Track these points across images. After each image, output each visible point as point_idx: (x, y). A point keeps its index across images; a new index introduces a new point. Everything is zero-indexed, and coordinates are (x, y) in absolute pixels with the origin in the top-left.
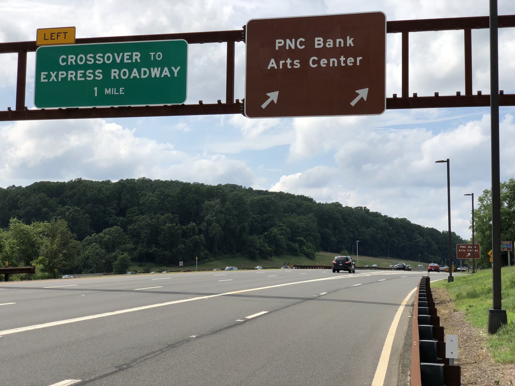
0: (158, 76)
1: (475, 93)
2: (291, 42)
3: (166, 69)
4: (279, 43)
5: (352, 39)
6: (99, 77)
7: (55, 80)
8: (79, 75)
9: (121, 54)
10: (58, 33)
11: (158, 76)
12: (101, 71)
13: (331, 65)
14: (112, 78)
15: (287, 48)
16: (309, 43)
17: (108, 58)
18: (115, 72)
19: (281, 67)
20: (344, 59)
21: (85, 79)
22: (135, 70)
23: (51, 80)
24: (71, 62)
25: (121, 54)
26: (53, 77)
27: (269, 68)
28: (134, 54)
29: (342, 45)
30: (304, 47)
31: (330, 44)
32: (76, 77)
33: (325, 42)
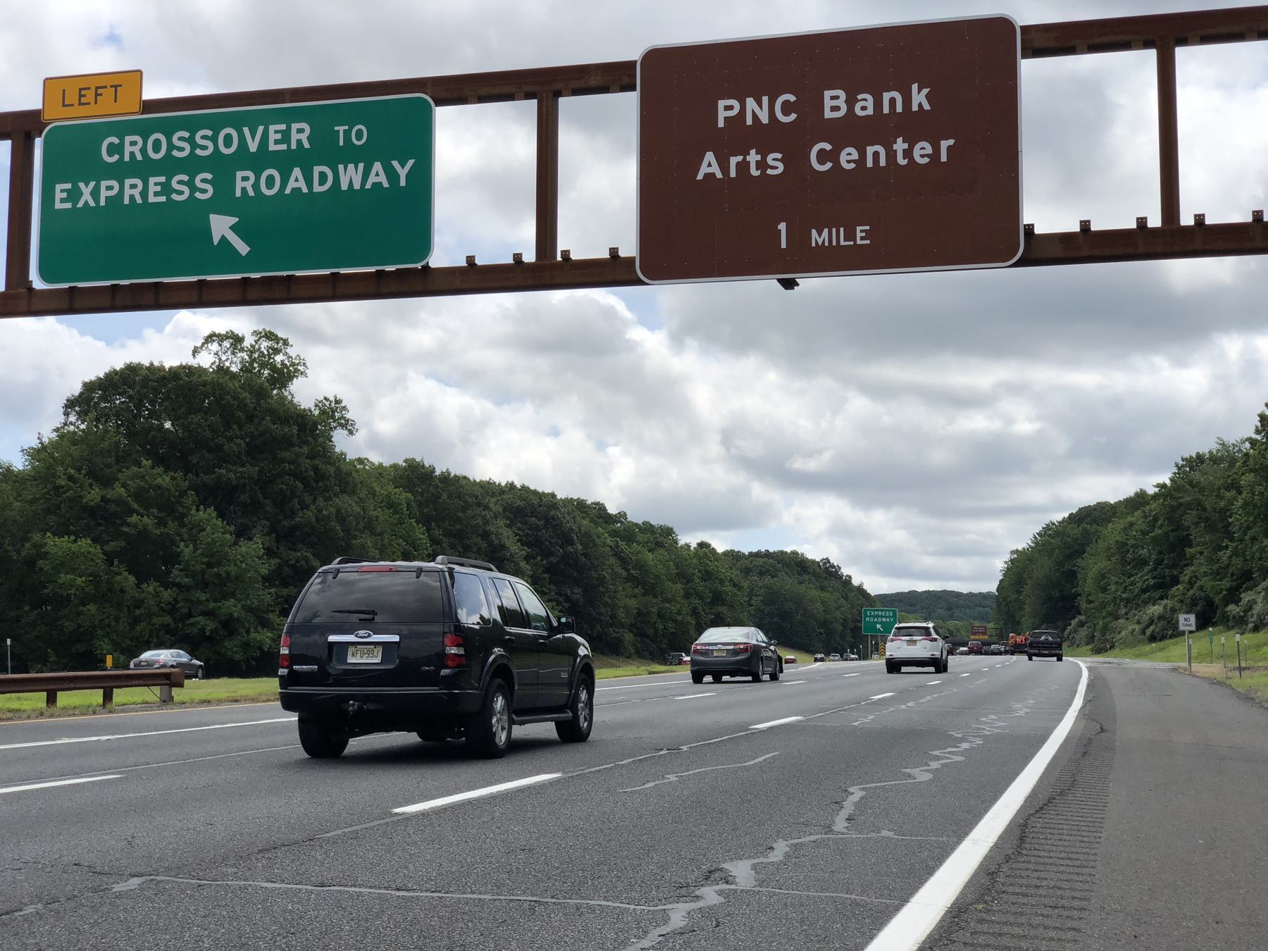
0: (357, 186)
1: (1187, 220)
2: (760, 104)
3: (377, 166)
4: (726, 109)
5: (925, 91)
6: (205, 191)
7: (92, 204)
8: (153, 189)
9: (261, 128)
10: (97, 88)
11: (357, 186)
12: (209, 176)
13: (870, 164)
14: (238, 194)
15: (749, 122)
16: (809, 105)
17: (228, 142)
18: (245, 179)
19: (733, 174)
20: (906, 146)
21: (169, 198)
22: (297, 172)
23: (80, 205)
24: (132, 154)
25: (261, 128)
26: (86, 196)
27: (700, 177)
28: (295, 126)
29: (899, 109)
30: (793, 116)
31: (865, 105)
32: (144, 194)
33: (851, 102)
